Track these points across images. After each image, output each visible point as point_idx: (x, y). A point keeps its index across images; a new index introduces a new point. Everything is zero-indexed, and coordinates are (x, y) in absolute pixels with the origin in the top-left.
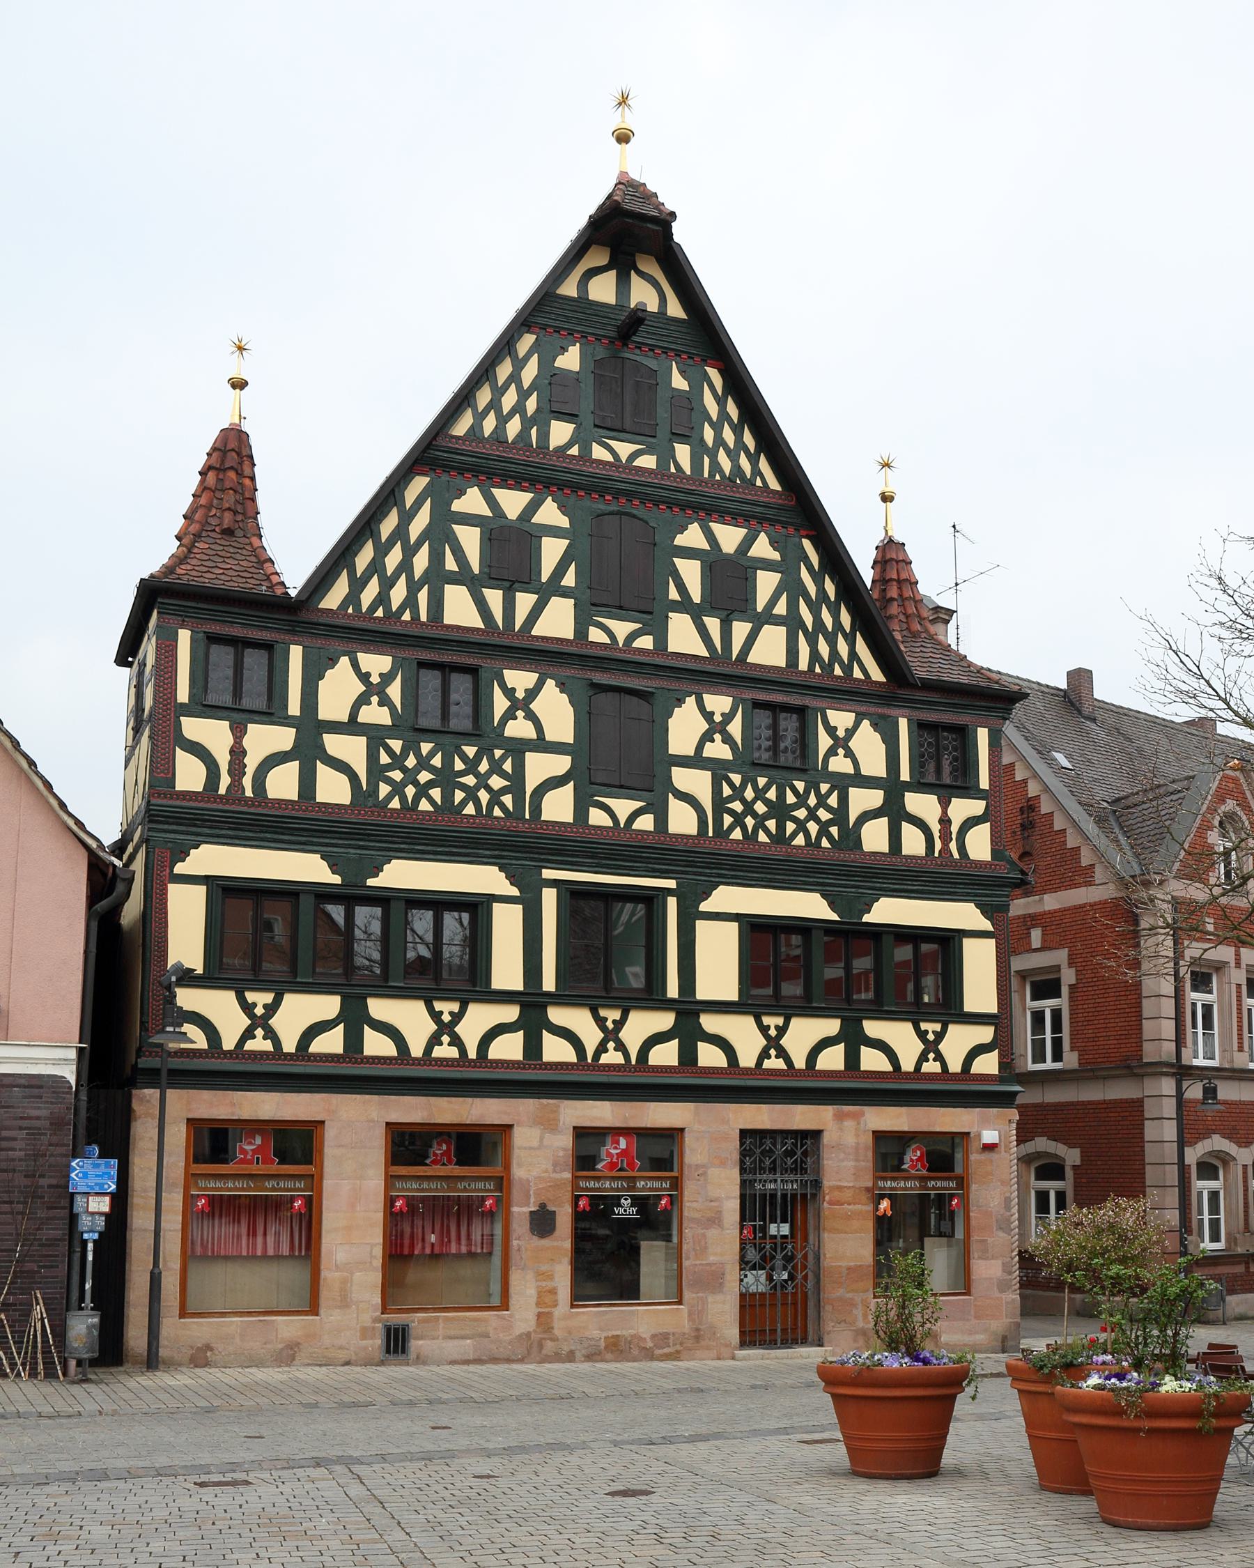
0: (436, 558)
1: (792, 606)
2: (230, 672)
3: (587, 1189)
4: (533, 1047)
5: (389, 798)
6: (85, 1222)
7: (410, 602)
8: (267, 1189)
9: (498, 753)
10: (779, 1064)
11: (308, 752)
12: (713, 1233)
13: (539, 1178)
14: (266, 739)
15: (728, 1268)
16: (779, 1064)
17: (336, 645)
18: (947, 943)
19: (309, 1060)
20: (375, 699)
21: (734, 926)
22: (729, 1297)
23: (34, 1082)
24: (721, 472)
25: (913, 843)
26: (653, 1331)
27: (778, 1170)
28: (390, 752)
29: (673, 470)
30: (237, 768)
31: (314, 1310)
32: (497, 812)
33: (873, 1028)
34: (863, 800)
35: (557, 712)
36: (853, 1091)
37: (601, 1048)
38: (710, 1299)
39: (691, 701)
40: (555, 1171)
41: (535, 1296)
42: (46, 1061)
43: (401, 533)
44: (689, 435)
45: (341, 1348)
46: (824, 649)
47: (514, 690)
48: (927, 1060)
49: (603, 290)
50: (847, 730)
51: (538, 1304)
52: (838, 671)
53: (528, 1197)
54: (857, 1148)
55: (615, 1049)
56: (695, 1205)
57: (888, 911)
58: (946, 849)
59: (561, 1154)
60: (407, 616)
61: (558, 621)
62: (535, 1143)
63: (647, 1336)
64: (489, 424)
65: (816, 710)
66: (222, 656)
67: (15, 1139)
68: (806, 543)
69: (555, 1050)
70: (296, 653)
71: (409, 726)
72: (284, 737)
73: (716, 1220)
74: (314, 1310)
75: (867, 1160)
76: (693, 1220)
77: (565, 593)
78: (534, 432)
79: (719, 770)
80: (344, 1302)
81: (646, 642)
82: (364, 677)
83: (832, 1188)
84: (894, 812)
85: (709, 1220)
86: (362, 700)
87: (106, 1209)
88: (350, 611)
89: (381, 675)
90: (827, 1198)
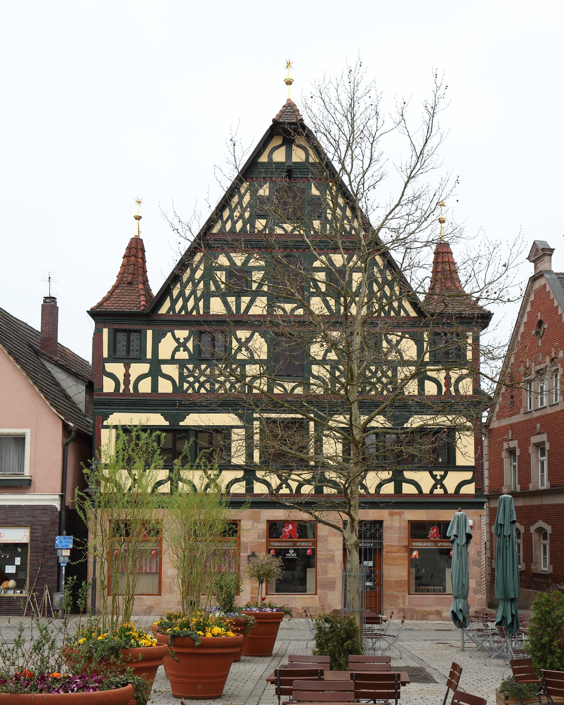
0: (207, 286)
2: (125, 343)
3: (274, 546)
5: (188, 389)
6: (61, 559)
7: (196, 307)
8: (298, 546)
9: (234, 366)
10: (441, 491)
11: (155, 373)
12: (330, 565)
13: (252, 542)
14: (138, 369)
15: (337, 580)
16: (441, 491)
17: (165, 328)
18: (225, 432)
20: (182, 349)
22: (337, 593)
23: (44, 508)
25: (431, 389)
26: (302, 606)
27: (363, 538)
28: (188, 369)
31: (160, 594)
33: (408, 475)
34: (403, 372)
35: (260, 346)
36: (399, 502)
38: (329, 593)
39: (169, 334)
40: (258, 539)
41: (250, 590)
42: (48, 500)
43: (191, 278)
44: (321, 216)
45: (170, 609)
47: (241, 339)
48: (437, 488)
49: (279, 156)
51: (251, 593)
52: (392, 314)
53: (247, 549)
54: (400, 528)
56: (322, 553)
57: (193, 420)
58: (448, 391)
59: (261, 531)
60: (194, 313)
61: (259, 307)
62: (250, 527)
63: (300, 608)
64: (228, 226)
66: (121, 337)
67: (38, 529)
69: (259, 488)
70: (149, 333)
71: (197, 357)
72: (145, 368)
73: (331, 559)
74: (160, 594)
75: (405, 533)
76: (321, 559)
77: (264, 294)
78: (248, 226)
79: (182, 364)
80: (171, 591)
81: (300, 312)
82: (177, 340)
83: (387, 546)
85: (328, 559)
86: (177, 350)
87: (69, 555)
88: (171, 313)
89: (184, 338)
90: (385, 550)
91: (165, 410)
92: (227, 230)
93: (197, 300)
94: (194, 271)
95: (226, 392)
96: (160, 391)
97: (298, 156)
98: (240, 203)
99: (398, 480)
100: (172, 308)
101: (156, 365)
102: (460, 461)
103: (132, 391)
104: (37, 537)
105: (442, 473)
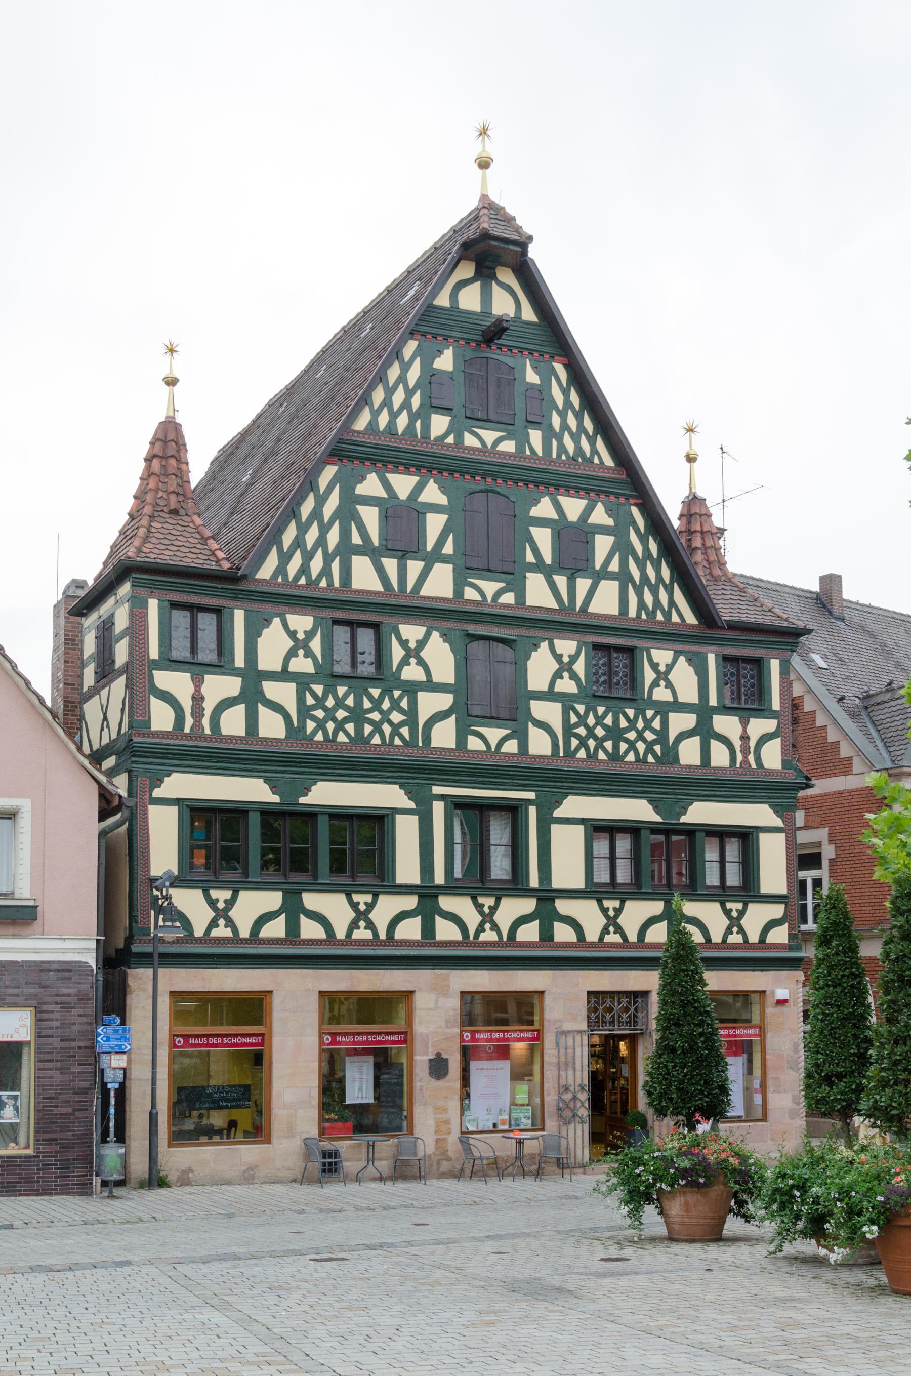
0: (345, 534)
1: (624, 564)
4: (428, 930)
7: (326, 571)
11: (252, 697)
14: (220, 686)
17: (268, 608)
18: (378, 822)
19: (260, 943)
20: (301, 652)
21: (581, 828)
24: (566, 452)
29: (528, 453)
30: (198, 712)
32: (397, 741)
33: (311, 900)
35: (441, 658)
37: (480, 929)
43: (316, 514)
46: (648, 598)
50: (667, 665)
51: (436, 1132)
52: (660, 617)
55: (491, 929)
58: (745, 761)
59: (452, 1013)
61: (440, 583)
62: (432, 1005)
64: (383, 420)
65: (642, 650)
66: (181, 619)
67: (53, 1012)
68: (635, 511)
70: (239, 616)
72: (231, 686)
77: (445, 560)
79: (302, 682)
82: (292, 634)
84: (705, 732)
86: (292, 653)
88: (280, 580)
89: (305, 632)
91: (272, 772)
92: (381, 429)
93: (328, 559)
94: (321, 501)
95: (638, 760)
96: (262, 734)
97: (503, 305)
98: (402, 379)
99: (293, 910)
100: (281, 569)
101: (253, 678)
102: (766, 887)
103: (207, 731)
104: (51, 1028)
105: (740, 906)
